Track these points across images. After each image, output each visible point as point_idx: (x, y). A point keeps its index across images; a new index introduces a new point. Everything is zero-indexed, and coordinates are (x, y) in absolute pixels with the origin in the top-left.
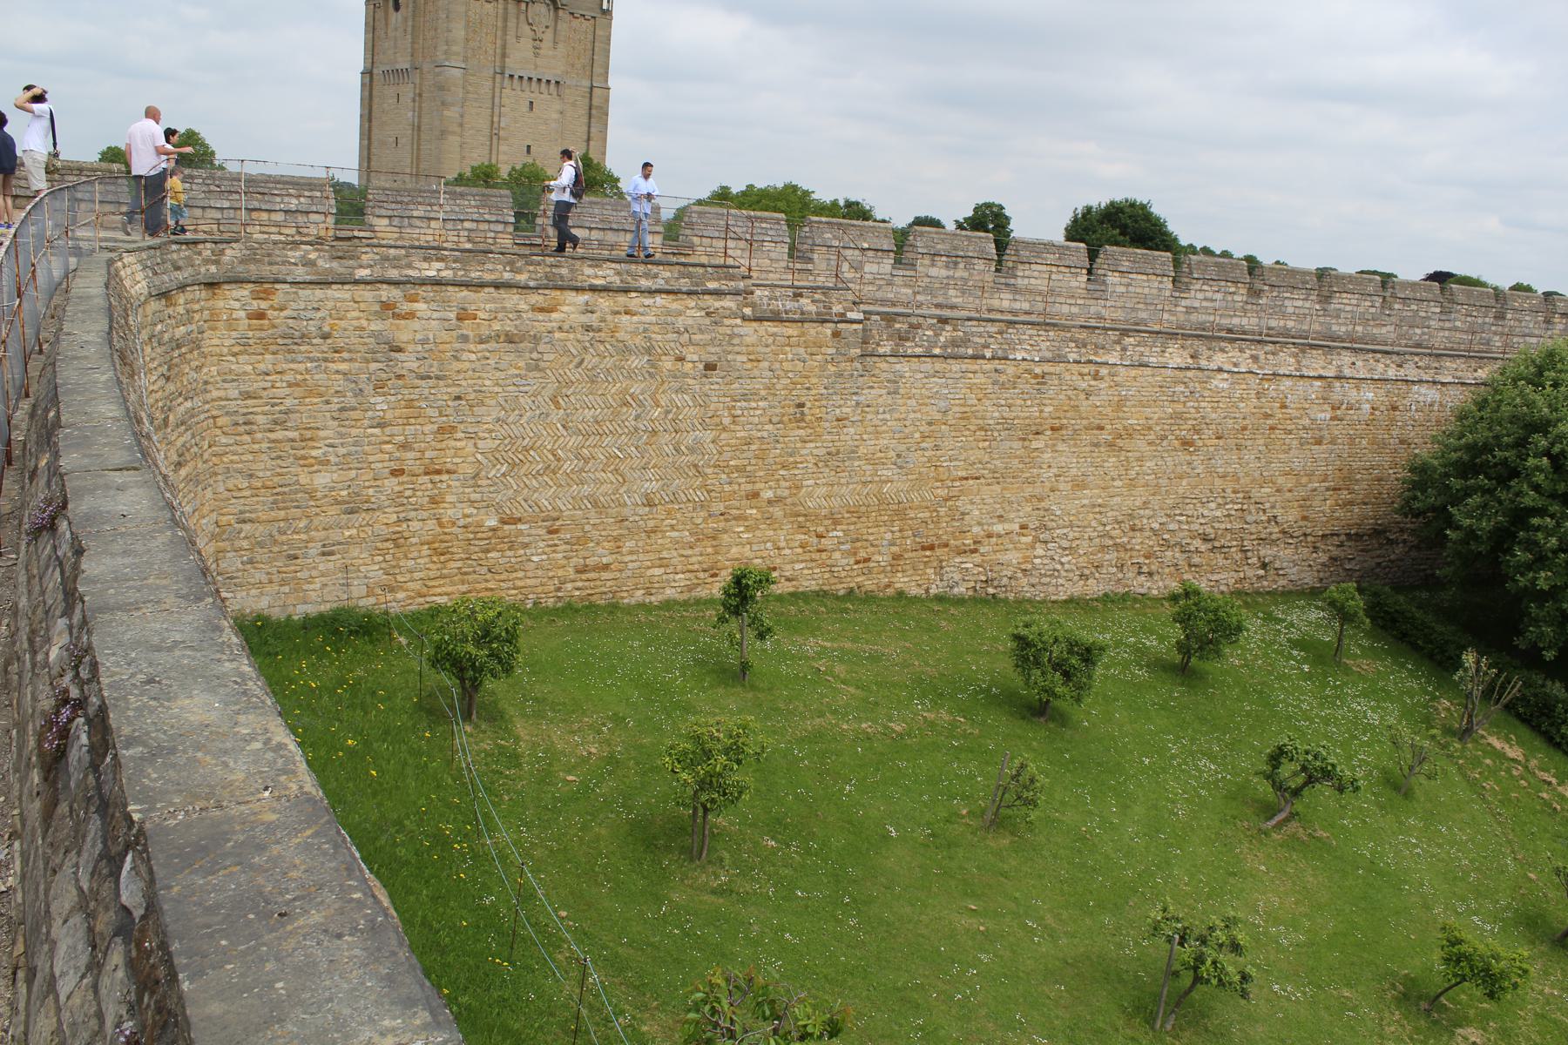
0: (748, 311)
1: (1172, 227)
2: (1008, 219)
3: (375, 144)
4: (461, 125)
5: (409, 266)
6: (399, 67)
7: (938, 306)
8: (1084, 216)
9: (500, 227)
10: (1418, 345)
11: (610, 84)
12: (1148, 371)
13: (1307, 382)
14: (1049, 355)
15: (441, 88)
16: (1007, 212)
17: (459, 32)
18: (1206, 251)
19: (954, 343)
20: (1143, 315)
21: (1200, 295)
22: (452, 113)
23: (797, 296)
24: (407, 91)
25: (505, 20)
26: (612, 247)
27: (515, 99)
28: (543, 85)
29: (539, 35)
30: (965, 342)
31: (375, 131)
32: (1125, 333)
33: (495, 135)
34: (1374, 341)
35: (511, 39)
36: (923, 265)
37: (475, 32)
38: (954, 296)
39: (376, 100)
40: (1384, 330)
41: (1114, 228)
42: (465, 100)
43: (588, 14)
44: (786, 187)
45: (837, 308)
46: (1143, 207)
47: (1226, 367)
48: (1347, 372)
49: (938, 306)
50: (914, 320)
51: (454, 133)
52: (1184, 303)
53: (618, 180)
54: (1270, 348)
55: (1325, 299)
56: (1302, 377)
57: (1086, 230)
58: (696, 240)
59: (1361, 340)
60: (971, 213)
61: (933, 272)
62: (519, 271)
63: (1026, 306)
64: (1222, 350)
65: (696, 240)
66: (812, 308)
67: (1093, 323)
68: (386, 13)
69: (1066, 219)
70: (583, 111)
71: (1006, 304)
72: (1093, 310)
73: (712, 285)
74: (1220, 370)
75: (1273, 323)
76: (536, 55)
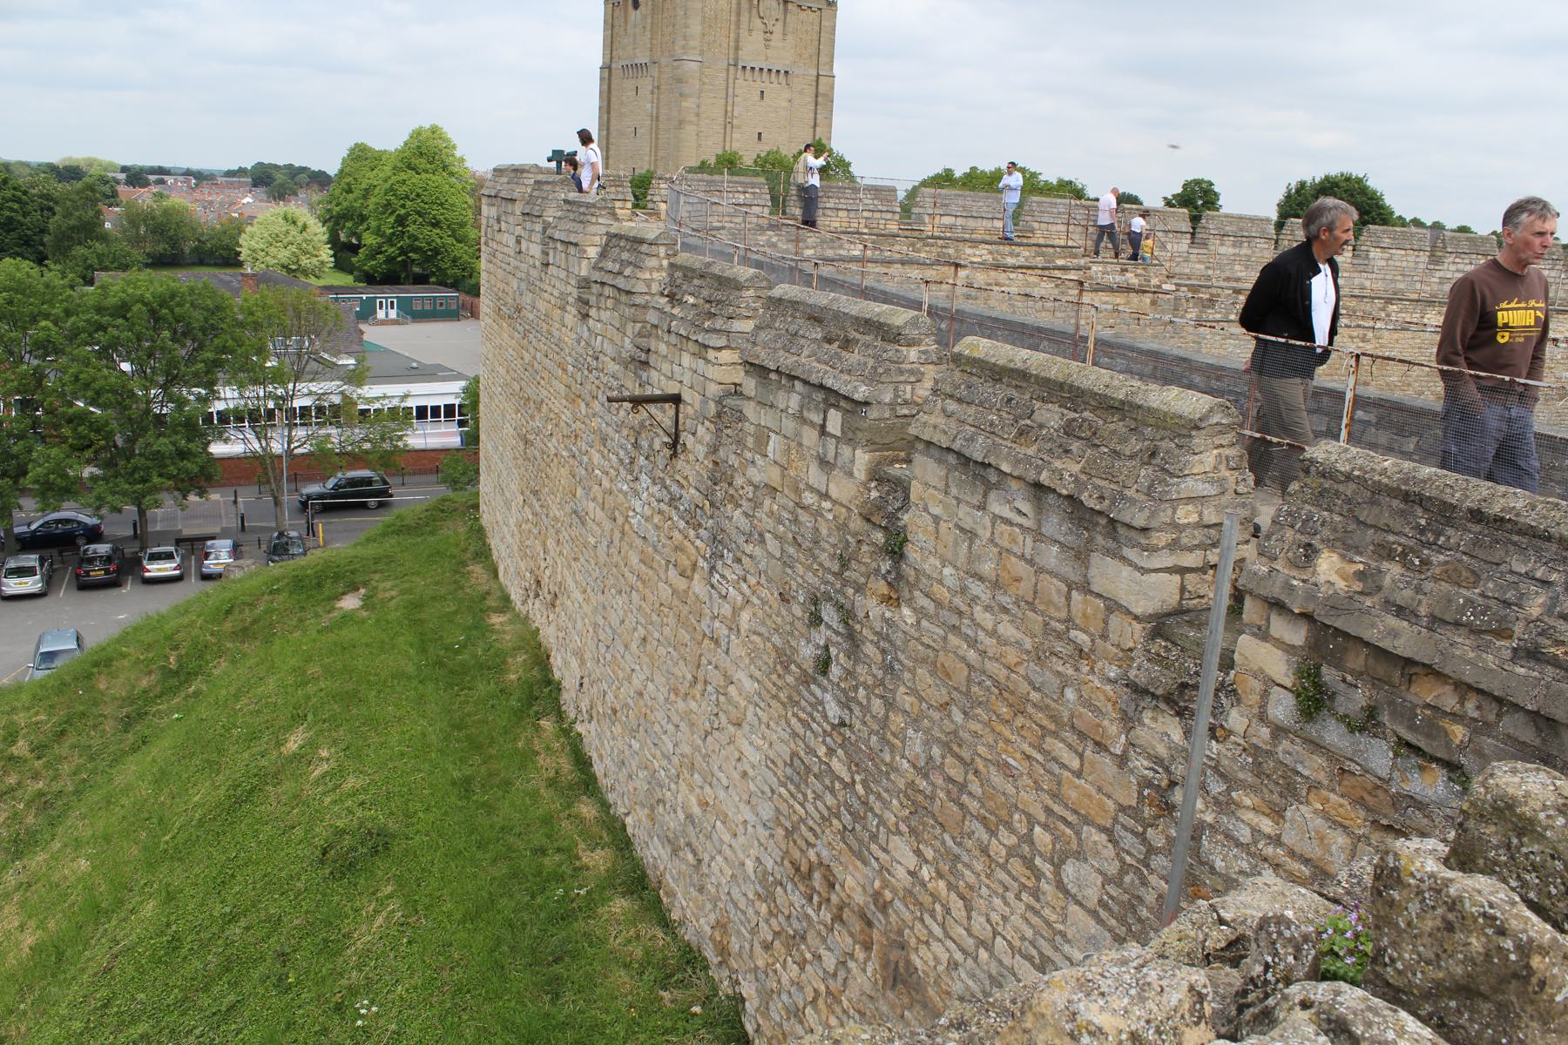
1: (1389, 200)
2: (1216, 195)
3: (613, 134)
5: (841, 247)
6: (638, 61)
7: (1228, 279)
8: (1298, 191)
9: (889, 216)
11: (835, 72)
15: (680, 81)
17: (695, 28)
18: (1417, 223)
20: (1401, 286)
21: (1452, 268)
22: (689, 104)
24: (646, 84)
25: (738, 14)
26: (973, 231)
27: (746, 88)
28: (757, 72)
29: (770, 28)
31: (613, 122)
32: (1389, 301)
33: (729, 124)
35: (744, 33)
36: (1214, 244)
39: (614, 93)
42: (701, 91)
43: (815, 6)
44: (1185, 186)
46: (1359, 181)
49: (1228, 279)
50: (1214, 291)
51: (691, 122)
52: (1438, 274)
53: (849, 164)
57: (1300, 205)
58: (1036, 225)
60: (1179, 190)
61: (1222, 250)
62: (919, 251)
65: (1036, 225)
67: (1356, 292)
68: (626, 12)
69: (1279, 195)
70: (810, 99)
72: (1356, 282)
73: (1060, 262)
76: (767, 47)
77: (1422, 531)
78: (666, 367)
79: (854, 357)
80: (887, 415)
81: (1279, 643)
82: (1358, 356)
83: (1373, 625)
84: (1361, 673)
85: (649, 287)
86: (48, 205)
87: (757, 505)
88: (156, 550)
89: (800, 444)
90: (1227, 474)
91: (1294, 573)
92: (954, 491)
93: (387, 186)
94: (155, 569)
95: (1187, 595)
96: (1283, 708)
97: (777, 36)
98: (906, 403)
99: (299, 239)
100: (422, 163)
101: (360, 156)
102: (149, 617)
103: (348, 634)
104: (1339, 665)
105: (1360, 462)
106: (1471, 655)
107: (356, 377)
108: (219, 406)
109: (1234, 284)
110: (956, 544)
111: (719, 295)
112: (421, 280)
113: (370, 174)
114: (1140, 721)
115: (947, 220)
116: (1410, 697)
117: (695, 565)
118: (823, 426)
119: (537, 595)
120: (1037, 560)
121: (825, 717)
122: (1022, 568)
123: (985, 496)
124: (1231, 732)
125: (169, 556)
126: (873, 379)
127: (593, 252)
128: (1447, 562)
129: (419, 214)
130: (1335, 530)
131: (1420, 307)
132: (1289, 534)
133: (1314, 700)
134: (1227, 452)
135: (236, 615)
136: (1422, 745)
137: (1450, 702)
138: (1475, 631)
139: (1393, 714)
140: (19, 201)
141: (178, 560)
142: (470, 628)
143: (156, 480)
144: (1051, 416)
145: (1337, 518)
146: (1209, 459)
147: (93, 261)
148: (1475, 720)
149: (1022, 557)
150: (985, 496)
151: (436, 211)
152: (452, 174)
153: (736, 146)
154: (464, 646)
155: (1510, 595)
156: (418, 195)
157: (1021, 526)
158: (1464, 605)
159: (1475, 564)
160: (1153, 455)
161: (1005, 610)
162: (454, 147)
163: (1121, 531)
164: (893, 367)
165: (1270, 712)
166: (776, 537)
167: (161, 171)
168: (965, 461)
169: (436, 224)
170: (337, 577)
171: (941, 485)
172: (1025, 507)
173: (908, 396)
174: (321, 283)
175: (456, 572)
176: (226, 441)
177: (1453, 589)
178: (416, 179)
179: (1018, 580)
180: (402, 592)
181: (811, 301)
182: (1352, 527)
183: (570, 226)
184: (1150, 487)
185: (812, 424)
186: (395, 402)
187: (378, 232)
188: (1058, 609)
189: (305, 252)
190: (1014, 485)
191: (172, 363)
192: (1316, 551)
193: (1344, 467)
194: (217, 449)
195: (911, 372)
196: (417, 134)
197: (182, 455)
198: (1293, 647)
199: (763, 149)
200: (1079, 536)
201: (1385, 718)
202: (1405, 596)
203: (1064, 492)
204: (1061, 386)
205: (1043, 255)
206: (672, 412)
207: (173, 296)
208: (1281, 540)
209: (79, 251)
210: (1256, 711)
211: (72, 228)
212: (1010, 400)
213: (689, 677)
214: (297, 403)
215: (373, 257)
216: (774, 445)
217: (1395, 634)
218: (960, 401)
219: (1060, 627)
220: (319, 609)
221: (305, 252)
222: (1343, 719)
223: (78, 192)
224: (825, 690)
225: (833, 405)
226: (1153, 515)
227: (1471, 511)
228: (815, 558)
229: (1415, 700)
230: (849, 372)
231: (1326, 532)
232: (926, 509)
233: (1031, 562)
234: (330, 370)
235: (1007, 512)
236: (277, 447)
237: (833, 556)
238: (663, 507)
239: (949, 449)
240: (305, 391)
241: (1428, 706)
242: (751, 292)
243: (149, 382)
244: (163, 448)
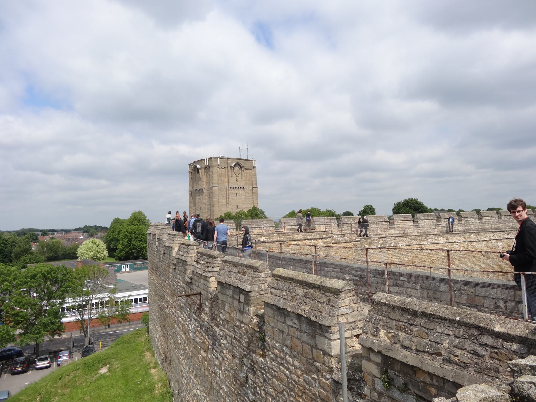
0: (333, 241)
2: (374, 209)
7: (376, 235)
8: (397, 205)
10: (512, 228)
12: (435, 245)
13: (481, 242)
14: (408, 244)
16: (374, 207)
19: (383, 243)
20: (430, 230)
23: (344, 236)
27: (232, 193)
30: (386, 243)
32: (427, 235)
33: (228, 204)
34: (498, 228)
35: (230, 178)
38: (379, 232)
40: (500, 225)
41: (407, 207)
45: (354, 238)
46: (415, 200)
47: (457, 241)
48: (492, 238)
49: (376, 235)
50: (372, 239)
54: (468, 234)
55: (481, 219)
56: (479, 241)
59: (494, 229)
60: (363, 209)
61: (373, 226)
63: (398, 232)
64: (454, 237)
66: (348, 239)
67: (417, 234)
69: (392, 207)
70: (251, 195)
71: (393, 232)
73: (324, 236)
74: (455, 242)
75: (467, 228)
77: (409, 320)
78: (197, 284)
79: (246, 277)
80: (257, 294)
81: (374, 362)
82: (386, 264)
83: (399, 354)
84: (400, 371)
85: (192, 259)
86: (14, 244)
87: (224, 327)
88: (41, 357)
89: (233, 306)
90: (354, 305)
91: (374, 338)
92: (276, 318)
93: (125, 230)
94: (40, 364)
95: (348, 347)
96: (379, 385)
98: (262, 290)
99: (97, 248)
100: (136, 222)
101: (117, 221)
102: (32, 384)
103: (102, 382)
104: (393, 369)
105: (388, 298)
106: (430, 362)
107: (113, 291)
108: (66, 306)
109: (378, 236)
110: (279, 336)
111: (210, 261)
112: (137, 258)
113: (120, 227)
114: (339, 393)
115: (289, 227)
116: (416, 379)
117: (208, 347)
118: (239, 300)
119: (166, 361)
120: (301, 339)
121: (249, 399)
122: (297, 342)
123: (285, 319)
124: (366, 396)
125: (46, 359)
126: (251, 284)
127: (176, 249)
128: (418, 330)
129: (136, 238)
130: (384, 322)
131: (437, 236)
132: (371, 324)
133: (389, 383)
134: (353, 298)
135: (63, 379)
136: (423, 396)
137: (428, 380)
138: (430, 354)
139: (412, 385)
140: (4, 244)
141: (49, 360)
142: (144, 376)
143: (43, 332)
144: (301, 291)
145: (384, 318)
146: (347, 301)
147: (28, 261)
148: (437, 386)
149: (297, 338)
150: (285, 319)
151: (140, 237)
152: (145, 225)
153: (230, 210)
154: (141, 382)
155: (438, 340)
156: (135, 232)
157: (295, 328)
158: (425, 345)
159: (426, 331)
160: (329, 302)
161: (295, 357)
162: (146, 217)
163: (323, 327)
164: (257, 279)
165: (376, 387)
166: (230, 337)
167: (53, 231)
168: (278, 308)
169: (141, 241)
170: (100, 362)
171: (272, 316)
172: (296, 322)
173: (263, 288)
174: (104, 261)
175: (141, 355)
176: (67, 317)
177: (421, 340)
178: (134, 227)
179: (297, 346)
180: (122, 365)
181: (234, 261)
182: (389, 320)
183: (170, 241)
184: (330, 312)
185: (236, 299)
186: (126, 299)
187: (122, 244)
188: (310, 355)
189: (99, 252)
190: (292, 315)
191: (51, 293)
192: (379, 330)
193: (383, 301)
194: (64, 320)
195: (263, 280)
196: (134, 214)
197: (52, 323)
198: (378, 363)
199: (238, 210)
200: (312, 330)
201: (410, 387)
202: (407, 343)
203: (306, 316)
204: (302, 281)
205: (319, 234)
206: (199, 298)
207: (52, 271)
208: (368, 327)
209: (23, 258)
210: (372, 387)
211: (21, 251)
212: (289, 287)
213: (209, 387)
214: (94, 302)
215: (121, 252)
216: (227, 306)
217: (406, 357)
218: (275, 289)
219: (311, 361)
220: (93, 374)
221: (99, 252)
222: (398, 388)
223: (24, 240)
224: (247, 389)
225: (241, 293)
226: (331, 321)
227: (422, 312)
228: (241, 343)
229: (418, 380)
230: (245, 282)
231: (381, 323)
232: (269, 324)
233: (300, 340)
234: (104, 290)
235: (292, 324)
236: (86, 317)
237: (245, 342)
238: (199, 329)
239: (273, 305)
240: (96, 297)
241: (422, 382)
242: (219, 259)
243: (42, 299)
244: (46, 321)
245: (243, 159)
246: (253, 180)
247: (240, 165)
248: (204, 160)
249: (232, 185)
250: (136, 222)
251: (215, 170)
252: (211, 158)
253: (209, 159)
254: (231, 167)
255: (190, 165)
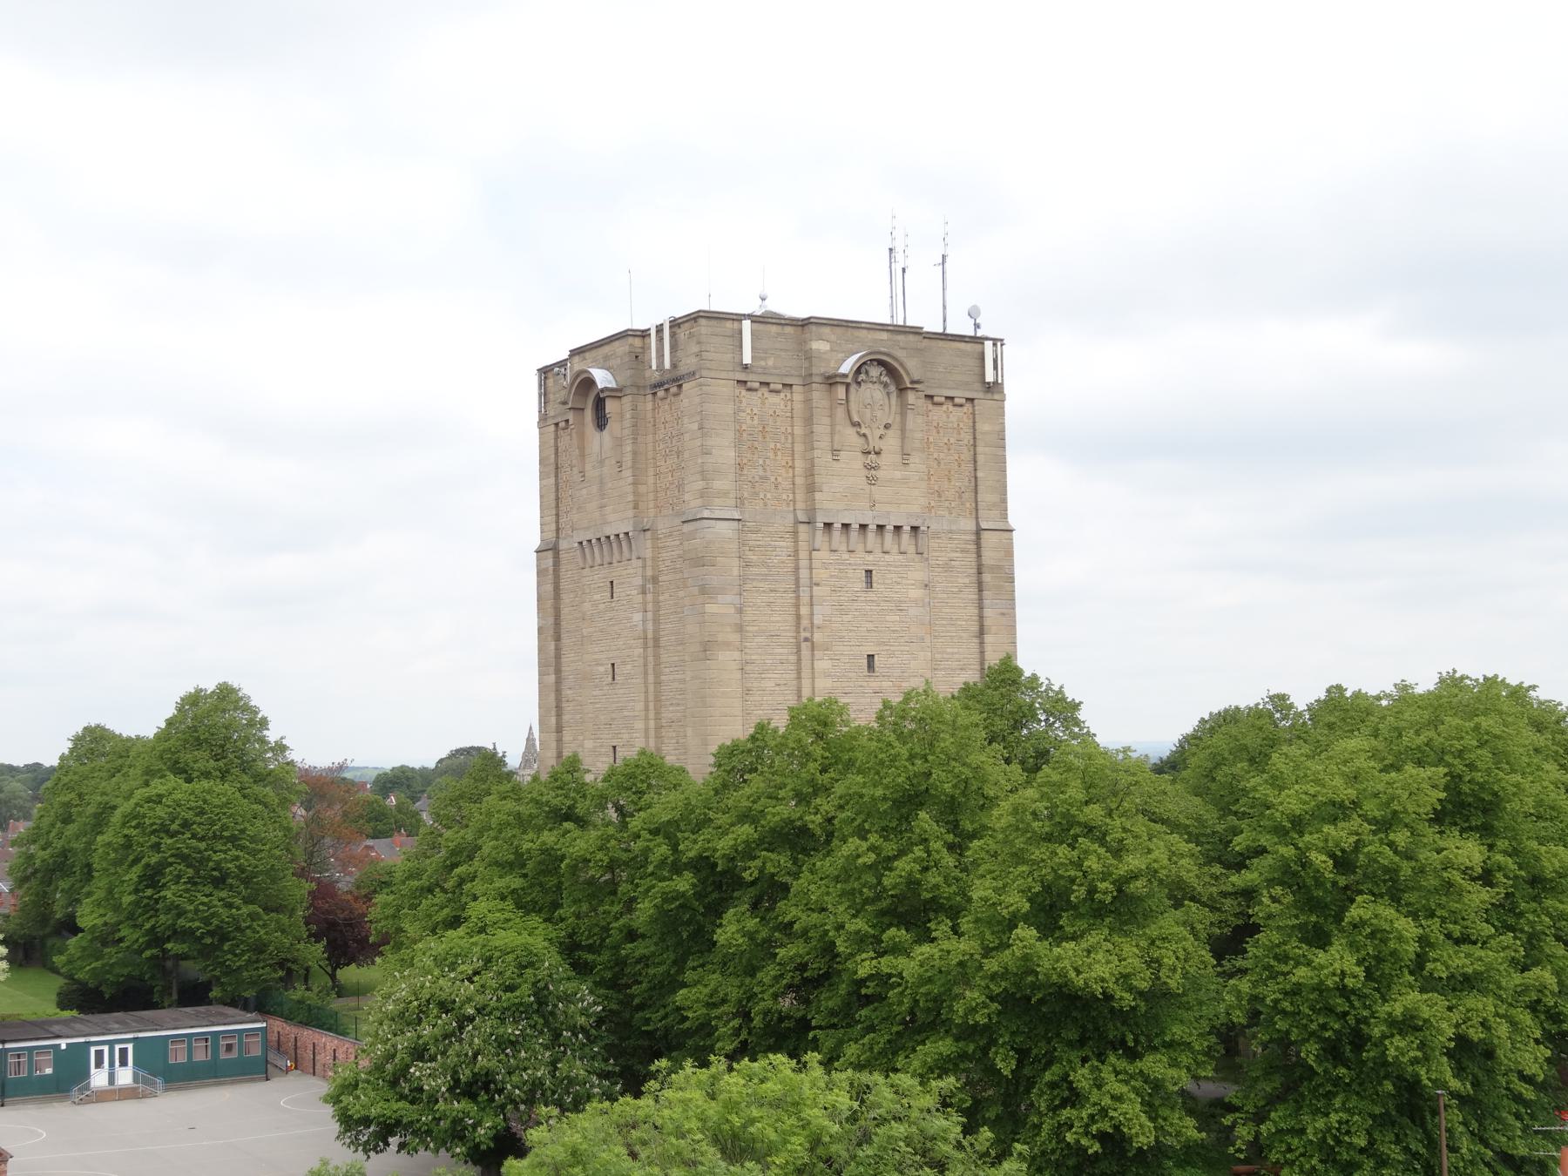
4: (740, 628)
27: (833, 567)
33: (804, 641)
35: (822, 457)
37: (753, 449)
68: (582, 436)
70: (966, 579)
76: (872, 481)
97: (889, 459)
100: (201, 760)
101: (94, 745)
129: (184, 858)
156: (186, 825)
162: (264, 723)
196: (193, 701)
245: (916, 331)
246: (978, 475)
247: (891, 371)
248: (644, 334)
249: (831, 505)
250: (201, 760)
251: (714, 395)
252: (695, 317)
253: (675, 324)
254: (831, 381)
255: (545, 372)
